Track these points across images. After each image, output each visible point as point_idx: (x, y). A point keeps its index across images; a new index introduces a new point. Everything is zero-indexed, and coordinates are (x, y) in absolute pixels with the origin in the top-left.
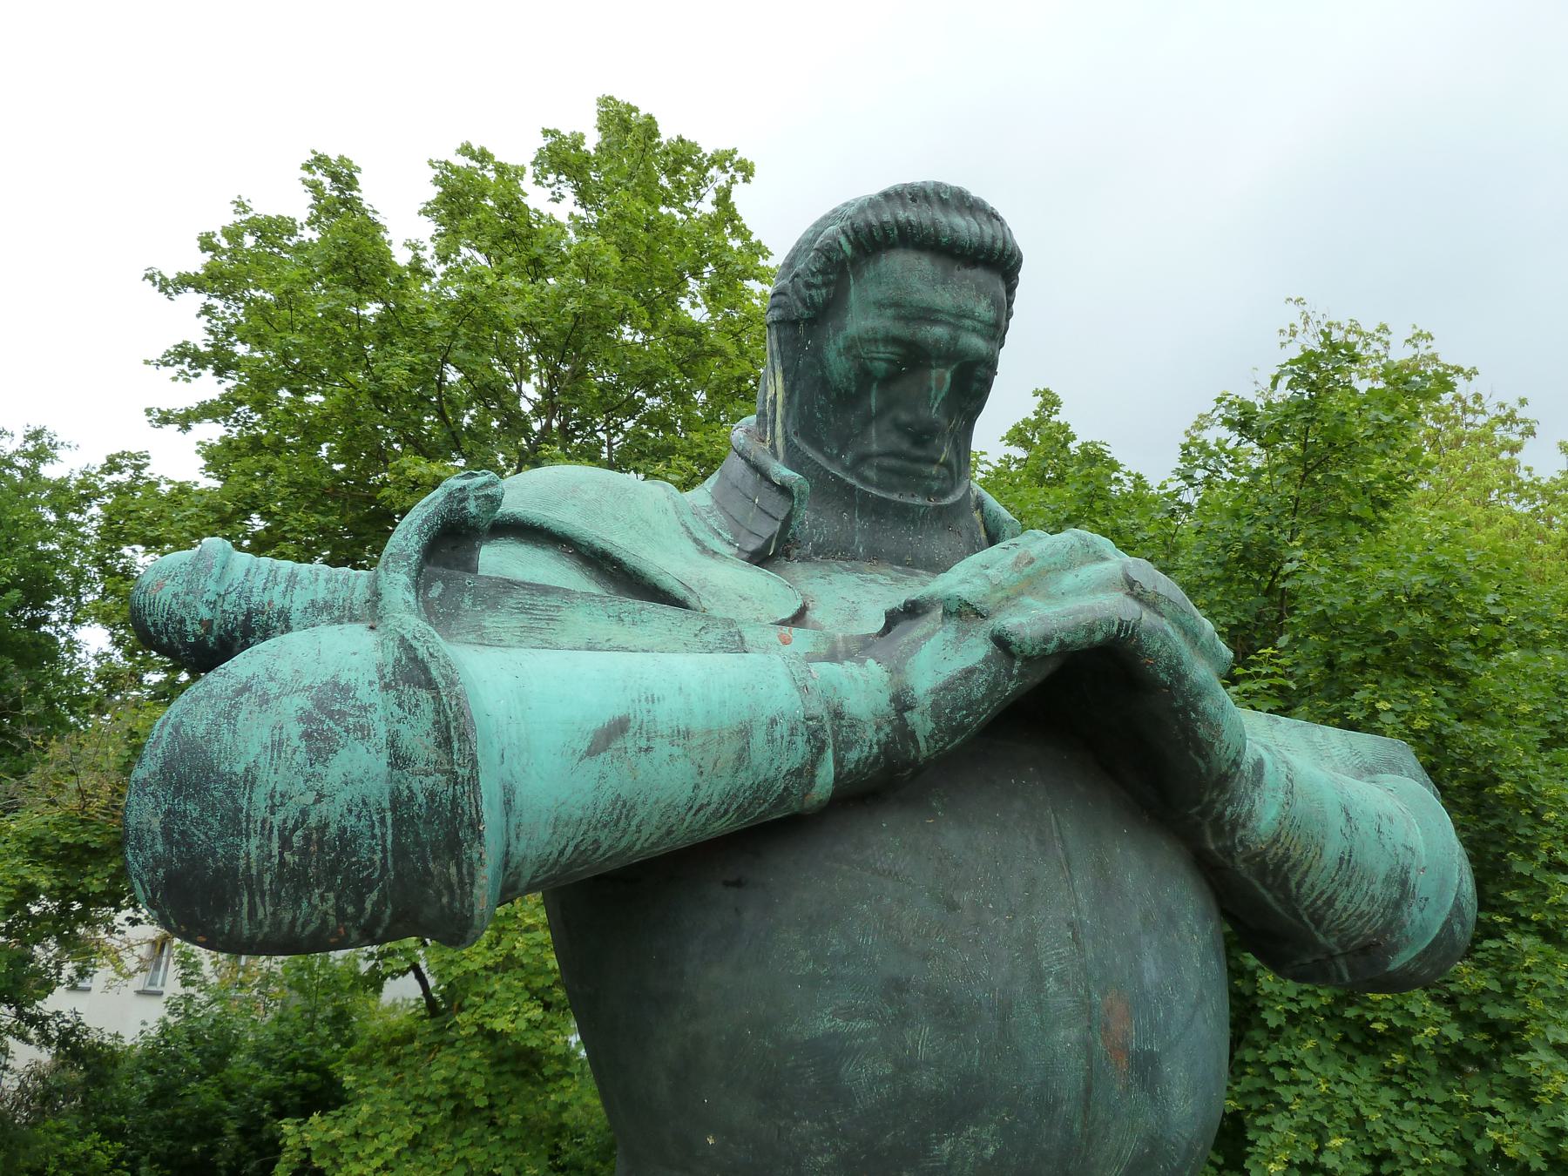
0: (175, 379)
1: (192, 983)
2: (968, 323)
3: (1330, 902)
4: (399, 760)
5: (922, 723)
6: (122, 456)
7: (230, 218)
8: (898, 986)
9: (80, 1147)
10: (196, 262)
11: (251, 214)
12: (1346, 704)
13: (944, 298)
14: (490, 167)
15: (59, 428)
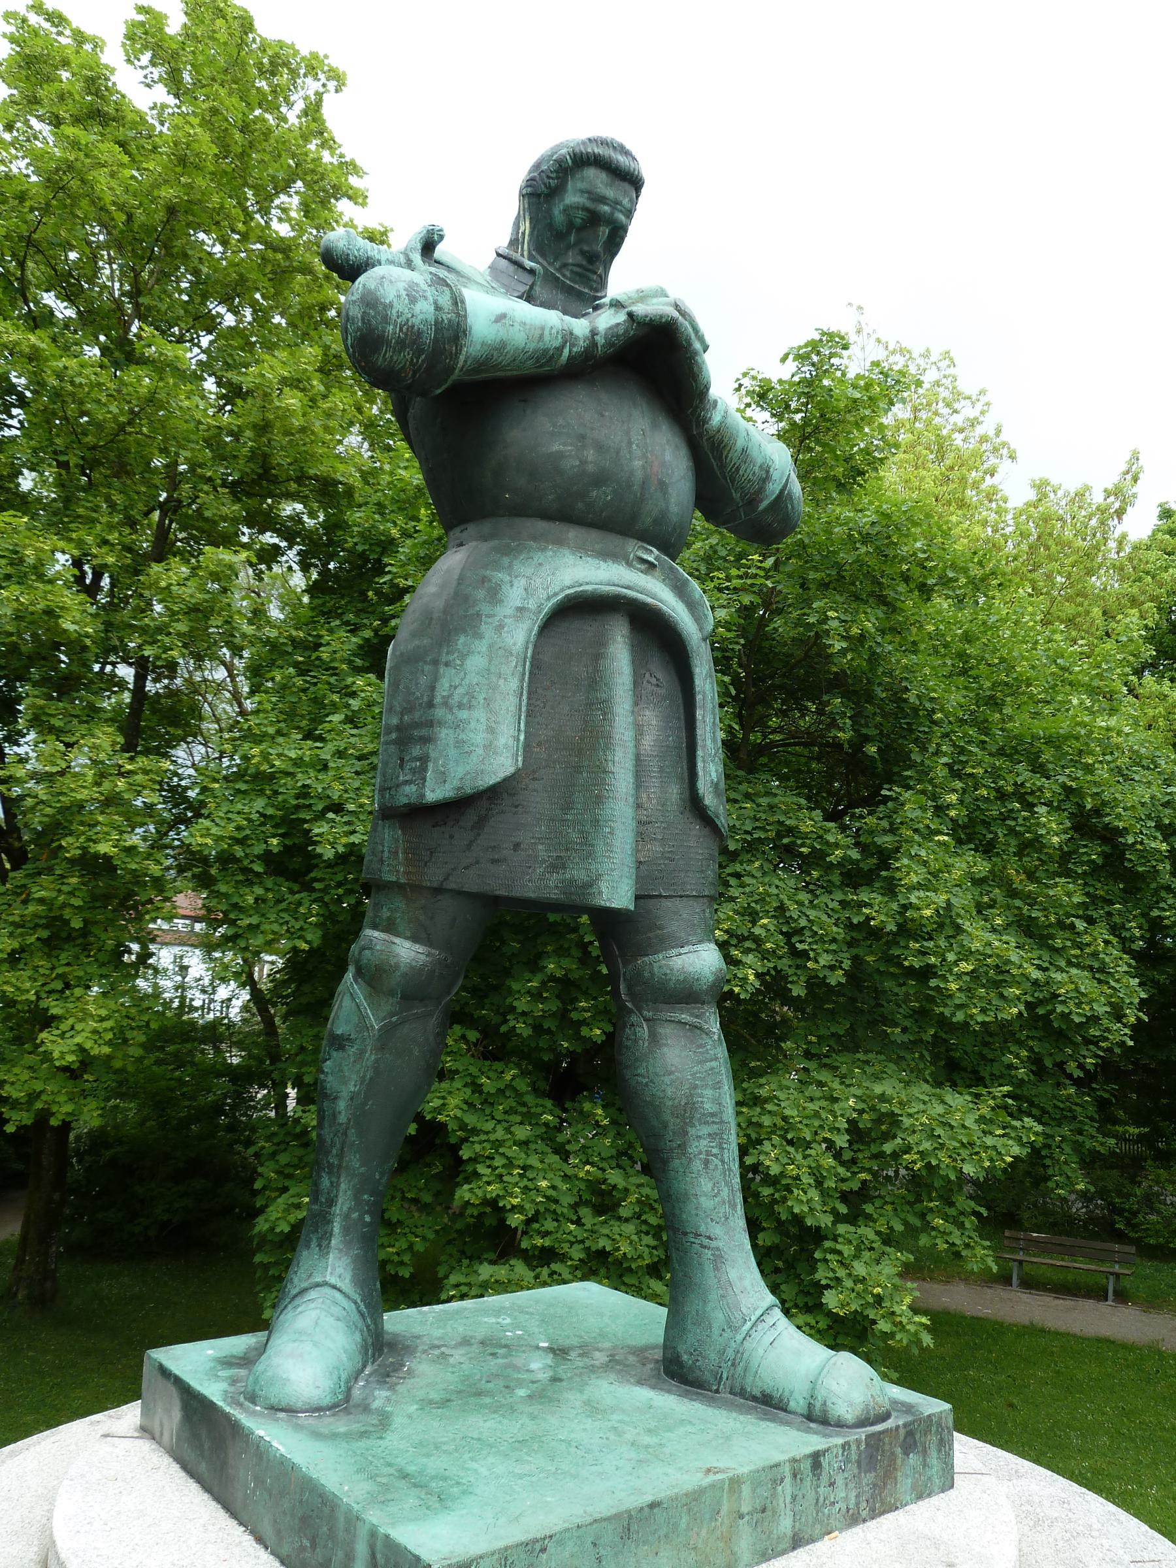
3: (738, 469)
4: (438, 308)
5: (600, 340)
12: (806, 611)
13: (610, 193)
14: (67, 32)
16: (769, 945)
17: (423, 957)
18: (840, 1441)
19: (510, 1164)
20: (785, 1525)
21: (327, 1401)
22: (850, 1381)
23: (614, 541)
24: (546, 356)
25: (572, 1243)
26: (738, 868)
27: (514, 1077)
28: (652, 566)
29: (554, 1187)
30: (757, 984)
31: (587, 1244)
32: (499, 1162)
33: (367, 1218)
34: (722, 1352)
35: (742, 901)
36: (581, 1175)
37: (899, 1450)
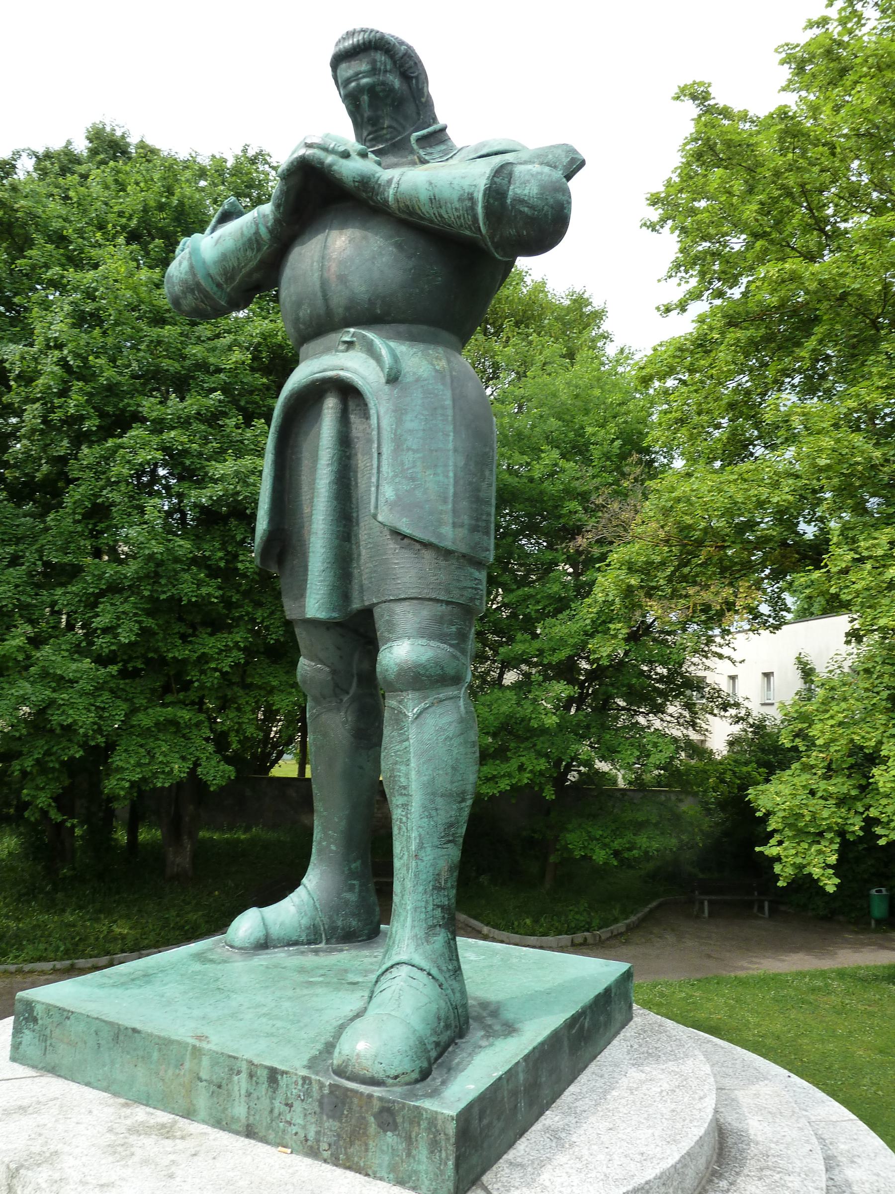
0: (679, 285)
9: (745, 769)
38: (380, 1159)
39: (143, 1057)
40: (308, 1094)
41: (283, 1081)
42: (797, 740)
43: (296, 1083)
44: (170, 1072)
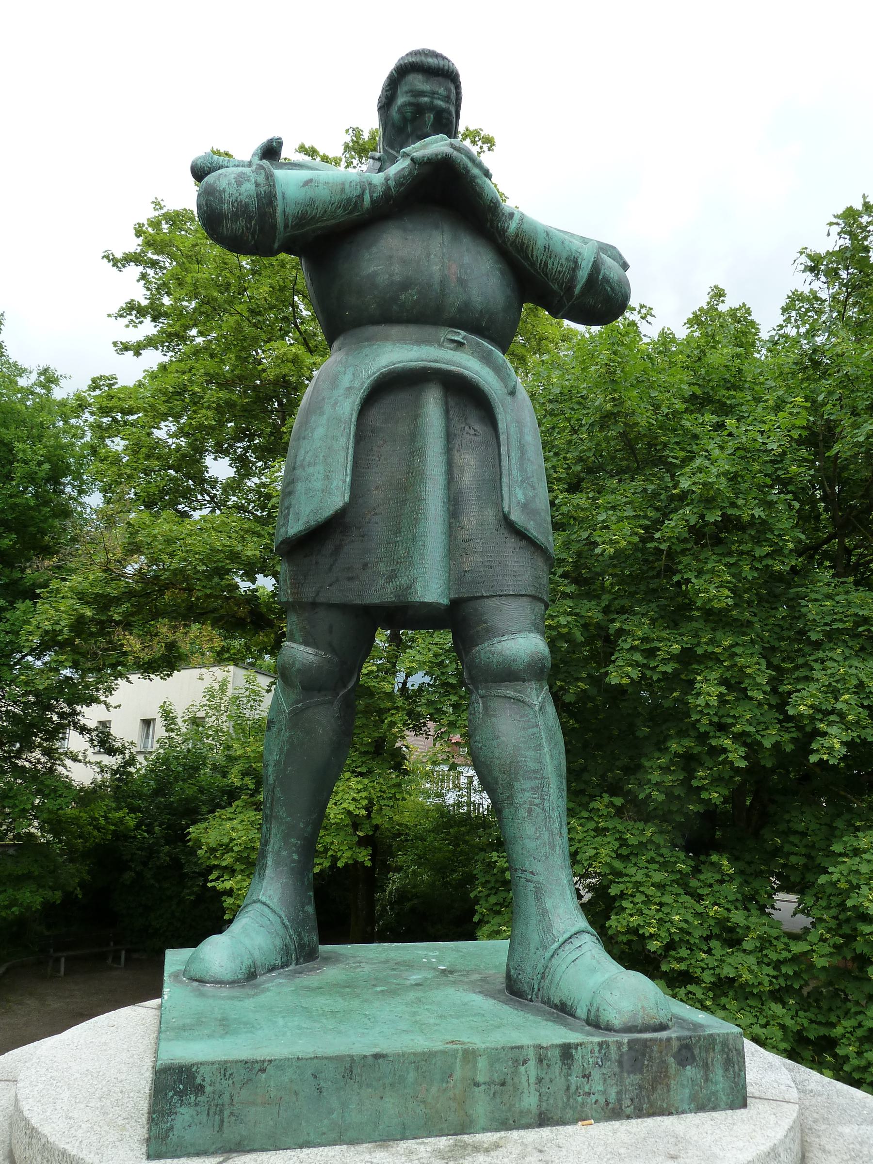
0: (127, 326)
1: (172, 730)
2: (436, 96)
3: (546, 264)
4: (257, 185)
6: (100, 378)
7: (152, 214)
8: (391, 257)
10: (133, 245)
11: (165, 210)
13: (426, 87)
15: (59, 368)
16: (850, 718)
17: (312, 657)
18: (597, 1039)
19: (648, 901)
20: (530, 1101)
21: (228, 977)
22: (630, 994)
23: (429, 330)
24: (351, 204)
25: (703, 969)
26: (821, 655)
27: (653, 834)
28: (460, 344)
29: (686, 921)
30: (844, 751)
31: (717, 971)
32: (640, 898)
33: (295, 857)
34: (535, 967)
35: (825, 680)
36: (711, 914)
37: (671, 1060)
38: (681, 1093)
39: (392, 1085)
40: (606, 1058)
41: (577, 1055)
42: (247, 778)
43: (592, 1051)
44: (434, 1090)
